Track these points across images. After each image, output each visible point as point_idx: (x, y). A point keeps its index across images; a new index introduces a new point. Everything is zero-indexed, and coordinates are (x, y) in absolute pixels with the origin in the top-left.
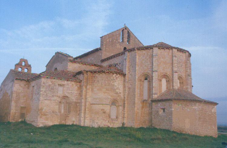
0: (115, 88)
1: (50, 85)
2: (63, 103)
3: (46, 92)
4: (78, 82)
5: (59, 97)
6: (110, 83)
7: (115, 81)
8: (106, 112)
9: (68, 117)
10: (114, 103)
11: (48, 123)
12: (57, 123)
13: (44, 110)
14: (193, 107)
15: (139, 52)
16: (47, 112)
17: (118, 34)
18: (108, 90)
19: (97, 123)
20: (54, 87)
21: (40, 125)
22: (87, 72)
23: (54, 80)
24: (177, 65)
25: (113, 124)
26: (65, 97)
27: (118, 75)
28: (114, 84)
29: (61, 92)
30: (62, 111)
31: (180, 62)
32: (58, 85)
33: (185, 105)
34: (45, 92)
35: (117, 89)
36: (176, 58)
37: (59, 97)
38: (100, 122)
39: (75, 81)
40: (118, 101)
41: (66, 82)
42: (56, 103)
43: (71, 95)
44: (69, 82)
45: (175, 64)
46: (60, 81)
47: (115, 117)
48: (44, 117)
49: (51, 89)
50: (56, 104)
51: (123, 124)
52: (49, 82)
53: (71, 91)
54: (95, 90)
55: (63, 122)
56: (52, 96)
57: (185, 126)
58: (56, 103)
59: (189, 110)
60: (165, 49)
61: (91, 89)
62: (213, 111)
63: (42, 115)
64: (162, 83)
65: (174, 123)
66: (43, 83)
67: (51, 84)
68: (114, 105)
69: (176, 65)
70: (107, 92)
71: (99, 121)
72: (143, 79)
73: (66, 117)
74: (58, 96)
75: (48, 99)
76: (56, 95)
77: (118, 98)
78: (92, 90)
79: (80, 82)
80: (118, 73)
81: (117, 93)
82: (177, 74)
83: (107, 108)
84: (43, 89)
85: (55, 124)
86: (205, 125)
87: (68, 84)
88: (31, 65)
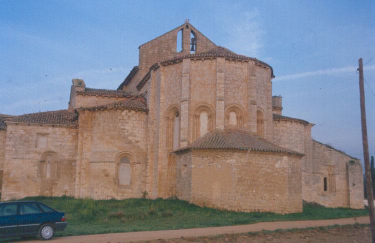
0: (126, 134)
1: (22, 136)
2: (49, 162)
3: (14, 147)
4: (72, 128)
5: (39, 153)
6: (116, 127)
9: (56, 184)
10: (124, 158)
11: (18, 194)
13: (11, 175)
15: (166, 69)
16: (18, 178)
17: (170, 38)
21: (6, 198)
22: (84, 110)
23: (28, 128)
24: (223, 86)
25: (121, 194)
26: (49, 153)
27: (133, 112)
28: (124, 127)
29: (44, 144)
30: (48, 175)
31: (235, 80)
32: (38, 134)
34: (13, 146)
35: (129, 135)
36: (223, 74)
37: (39, 153)
38: (102, 192)
39: (67, 127)
40: (131, 156)
41: (50, 130)
42: (34, 163)
43: (61, 148)
44: (57, 129)
45: (221, 86)
46: (40, 128)
47: (128, 183)
48: (13, 186)
49: (25, 141)
51: (145, 193)
53: (60, 143)
54: (95, 139)
56: (27, 152)
58: (34, 163)
59: (219, 166)
60: (203, 59)
61: (90, 138)
62: (277, 166)
63: (8, 182)
64: (201, 121)
66: (10, 132)
67: (24, 133)
69: (222, 87)
70: (111, 143)
71: (99, 189)
72: (172, 115)
73: (53, 183)
74: (36, 152)
75: (19, 156)
76: (33, 151)
77: (133, 151)
78: (92, 139)
79: (76, 128)
80: (293, 121)
81: (130, 142)
82: (256, 106)
83: (111, 169)
84: (9, 143)
85: (32, 195)
86: (254, 191)
87: (54, 133)
88: (280, 97)
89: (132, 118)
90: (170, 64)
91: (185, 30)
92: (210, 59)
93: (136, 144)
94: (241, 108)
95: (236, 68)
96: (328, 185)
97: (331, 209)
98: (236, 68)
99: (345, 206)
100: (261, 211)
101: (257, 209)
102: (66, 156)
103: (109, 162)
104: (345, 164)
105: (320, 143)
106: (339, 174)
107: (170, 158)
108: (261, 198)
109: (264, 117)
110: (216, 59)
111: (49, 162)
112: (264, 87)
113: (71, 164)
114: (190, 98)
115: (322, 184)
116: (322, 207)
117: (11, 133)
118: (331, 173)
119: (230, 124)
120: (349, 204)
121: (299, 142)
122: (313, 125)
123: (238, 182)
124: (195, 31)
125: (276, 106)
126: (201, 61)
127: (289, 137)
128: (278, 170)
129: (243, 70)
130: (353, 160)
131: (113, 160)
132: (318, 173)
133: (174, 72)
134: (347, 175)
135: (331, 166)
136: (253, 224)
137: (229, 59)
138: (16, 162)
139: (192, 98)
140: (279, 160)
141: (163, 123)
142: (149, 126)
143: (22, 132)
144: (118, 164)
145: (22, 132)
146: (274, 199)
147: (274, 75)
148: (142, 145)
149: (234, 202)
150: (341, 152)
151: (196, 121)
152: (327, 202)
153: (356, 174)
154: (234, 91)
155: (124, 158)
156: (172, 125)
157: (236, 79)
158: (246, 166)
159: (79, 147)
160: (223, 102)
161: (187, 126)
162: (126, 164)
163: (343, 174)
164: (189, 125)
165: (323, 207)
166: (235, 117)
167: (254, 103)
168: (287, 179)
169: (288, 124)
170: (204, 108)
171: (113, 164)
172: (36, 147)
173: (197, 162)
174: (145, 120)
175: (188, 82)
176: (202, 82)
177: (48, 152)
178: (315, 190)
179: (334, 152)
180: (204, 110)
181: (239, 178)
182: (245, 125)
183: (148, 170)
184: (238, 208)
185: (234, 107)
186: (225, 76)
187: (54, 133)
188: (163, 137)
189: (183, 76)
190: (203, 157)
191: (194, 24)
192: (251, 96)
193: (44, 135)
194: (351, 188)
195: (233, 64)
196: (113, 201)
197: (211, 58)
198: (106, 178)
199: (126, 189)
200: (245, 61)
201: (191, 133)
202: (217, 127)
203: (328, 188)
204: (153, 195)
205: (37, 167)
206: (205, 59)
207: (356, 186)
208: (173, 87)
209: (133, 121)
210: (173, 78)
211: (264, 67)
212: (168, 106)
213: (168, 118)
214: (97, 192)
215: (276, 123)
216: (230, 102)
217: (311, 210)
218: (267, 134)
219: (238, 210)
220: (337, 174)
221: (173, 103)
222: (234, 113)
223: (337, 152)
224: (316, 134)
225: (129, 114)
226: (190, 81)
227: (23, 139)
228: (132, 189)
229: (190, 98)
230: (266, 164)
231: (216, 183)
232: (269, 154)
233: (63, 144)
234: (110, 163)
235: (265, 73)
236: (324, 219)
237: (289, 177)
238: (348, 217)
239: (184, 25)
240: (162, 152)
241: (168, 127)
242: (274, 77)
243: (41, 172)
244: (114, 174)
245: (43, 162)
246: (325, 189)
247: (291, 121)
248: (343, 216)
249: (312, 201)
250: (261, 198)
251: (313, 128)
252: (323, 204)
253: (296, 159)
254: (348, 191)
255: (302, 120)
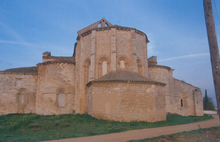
0: (62, 77)
1: (7, 80)
2: (23, 94)
3: (4, 86)
4: (35, 75)
5: (17, 89)
7: (62, 70)
8: (53, 100)
9: (26, 106)
10: (61, 91)
12: (14, 112)
14: (115, 89)
15: (84, 38)
16: (5, 103)
18: (55, 80)
19: (46, 111)
20: (12, 81)
23: (11, 75)
26: (22, 89)
28: (61, 73)
29: (20, 84)
30: (23, 102)
33: (106, 87)
34: (3, 86)
35: (64, 77)
36: (115, 37)
39: (32, 74)
41: (23, 76)
44: (26, 76)
45: (114, 44)
46: (18, 75)
47: (64, 105)
49: (9, 83)
50: (14, 95)
51: (74, 111)
52: (7, 77)
53: (28, 84)
54: (46, 80)
55: (21, 112)
57: (105, 111)
59: (109, 92)
61: (43, 80)
65: (94, 108)
67: (9, 78)
68: (63, 93)
69: (115, 45)
73: (25, 106)
78: (44, 81)
80: (161, 67)
81: (64, 81)
82: (136, 56)
86: (133, 108)
87: (25, 78)
89: (66, 68)
90: (85, 35)
91: (102, 23)
92: (107, 29)
93: (68, 83)
94: (127, 58)
95: (123, 34)
96: (183, 103)
97: (185, 117)
98: (123, 34)
99: (193, 115)
100: (138, 121)
101: (135, 119)
102: (32, 90)
103: (52, 93)
104: (192, 91)
105: (178, 80)
106: (189, 97)
107: (86, 89)
108: (138, 112)
109: (142, 63)
110: (110, 29)
111: (23, 94)
112: (142, 45)
113: (34, 95)
114: (96, 53)
115: (180, 103)
116: (180, 116)
117: (2, 79)
118: (185, 97)
119: (120, 67)
120: (195, 113)
121: (165, 79)
122: (173, 70)
123: (122, 102)
124: (107, 23)
125: (154, 61)
126: (102, 31)
127: (158, 75)
128: (149, 94)
129: (128, 35)
130: (197, 89)
131: (55, 92)
132: (177, 97)
133: (88, 39)
134: (194, 97)
135: (184, 93)
136: (123, 132)
137: (118, 29)
138: (5, 94)
139: (97, 53)
140: (149, 87)
141: (82, 70)
142: (76, 72)
143: (8, 78)
144: (58, 94)
145: (8, 78)
146: (146, 113)
147: (149, 40)
148: (71, 83)
149: (119, 115)
150: (190, 85)
151: (100, 67)
152: (184, 113)
153: (198, 96)
154: (122, 48)
155: (61, 91)
156: (87, 70)
157: (123, 40)
158: (127, 92)
159: (38, 85)
160: (115, 54)
161: (94, 70)
162: (62, 94)
163: (192, 97)
164: (95, 69)
165: (181, 116)
166: (124, 63)
167: (135, 54)
168: (154, 99)
169: (159, 69)
170: (104, 58)
171: (54, 94)
172: (15, 86)
173: (95, 90)
174: (74, 69)
175: (94, 43)
176: (103, 43)
177: (22, 88)
178: (176, 106)
179: (186, 84)
180: (105, 60)
181: (122, 100)
182: (130, 68)
183: (75, 98)
184: (122, 119)
185: (123, 57)
186: (116, 39)
187: (25, 78)
188: (82, 77)
189: (92, 40)
190: (99, 87)
191: (107, 19)
192: (133, 50)
193: (20, 79)
194: (196, 104)
195: (121, 32)
196: (54, 115)
197: (108, 29)
198: (50, 102)
199: (62, 108)
200: (129, 30)
201: (97, 74)
202: (112, 69)
203: (183, 105)
204: (78, 112)
205: (16, 97)
206: (104, 30)
207: (199, 103)
208: (87, 48)
209: (67, 69)
210: (87, 43)
211: (141, 34)
212: (85, 59)
213: (85, 66)
214: (46, 111)
215: (152, 69)
216: (120, 54)
217: (172, 119)
218: (144, 73)
219: (122, 121)
220: (188, 97)
221: (88, 57)
222: (123, 61)
223: (188, 85)
224: (176, 75)
225: (64, 65)
226: (96, 43)
227: (8, 82)
228: (66, 109)
229: (96, 53)
230: (140, 90)
231: (108, 104)
232: (142, 84)
233: (30, 84)
234: (53, 94)
235: (143, 38)
236: (178, 124)
237: (156, 98)
238: (194, 122)
239: (102, 20)
240: (82, 86)
241: (85, 72)
242: (149, 42)
243: (18, 100)
244: (55, 100)
245: (19, 94)
246: (182, 106)
247: (160, 67)
248: (191, 121)
249: (174, 113)
250: (138, 112)
251: (173, 72)
252: (181, 114)
253: (161, 87)
254: (195, 106)
255: (167, 67)
